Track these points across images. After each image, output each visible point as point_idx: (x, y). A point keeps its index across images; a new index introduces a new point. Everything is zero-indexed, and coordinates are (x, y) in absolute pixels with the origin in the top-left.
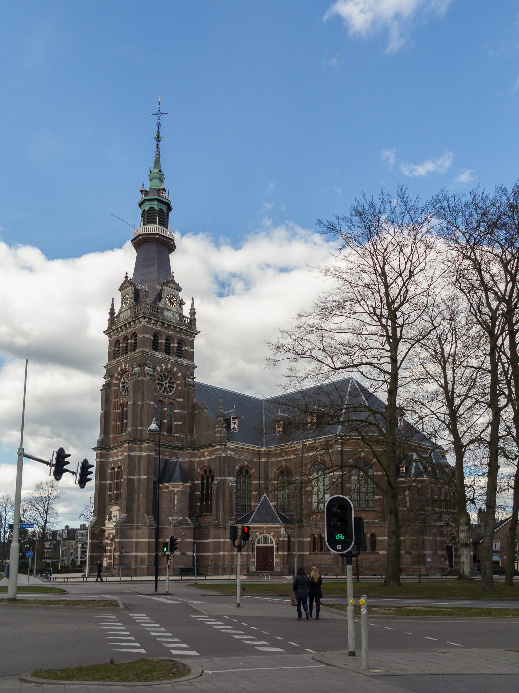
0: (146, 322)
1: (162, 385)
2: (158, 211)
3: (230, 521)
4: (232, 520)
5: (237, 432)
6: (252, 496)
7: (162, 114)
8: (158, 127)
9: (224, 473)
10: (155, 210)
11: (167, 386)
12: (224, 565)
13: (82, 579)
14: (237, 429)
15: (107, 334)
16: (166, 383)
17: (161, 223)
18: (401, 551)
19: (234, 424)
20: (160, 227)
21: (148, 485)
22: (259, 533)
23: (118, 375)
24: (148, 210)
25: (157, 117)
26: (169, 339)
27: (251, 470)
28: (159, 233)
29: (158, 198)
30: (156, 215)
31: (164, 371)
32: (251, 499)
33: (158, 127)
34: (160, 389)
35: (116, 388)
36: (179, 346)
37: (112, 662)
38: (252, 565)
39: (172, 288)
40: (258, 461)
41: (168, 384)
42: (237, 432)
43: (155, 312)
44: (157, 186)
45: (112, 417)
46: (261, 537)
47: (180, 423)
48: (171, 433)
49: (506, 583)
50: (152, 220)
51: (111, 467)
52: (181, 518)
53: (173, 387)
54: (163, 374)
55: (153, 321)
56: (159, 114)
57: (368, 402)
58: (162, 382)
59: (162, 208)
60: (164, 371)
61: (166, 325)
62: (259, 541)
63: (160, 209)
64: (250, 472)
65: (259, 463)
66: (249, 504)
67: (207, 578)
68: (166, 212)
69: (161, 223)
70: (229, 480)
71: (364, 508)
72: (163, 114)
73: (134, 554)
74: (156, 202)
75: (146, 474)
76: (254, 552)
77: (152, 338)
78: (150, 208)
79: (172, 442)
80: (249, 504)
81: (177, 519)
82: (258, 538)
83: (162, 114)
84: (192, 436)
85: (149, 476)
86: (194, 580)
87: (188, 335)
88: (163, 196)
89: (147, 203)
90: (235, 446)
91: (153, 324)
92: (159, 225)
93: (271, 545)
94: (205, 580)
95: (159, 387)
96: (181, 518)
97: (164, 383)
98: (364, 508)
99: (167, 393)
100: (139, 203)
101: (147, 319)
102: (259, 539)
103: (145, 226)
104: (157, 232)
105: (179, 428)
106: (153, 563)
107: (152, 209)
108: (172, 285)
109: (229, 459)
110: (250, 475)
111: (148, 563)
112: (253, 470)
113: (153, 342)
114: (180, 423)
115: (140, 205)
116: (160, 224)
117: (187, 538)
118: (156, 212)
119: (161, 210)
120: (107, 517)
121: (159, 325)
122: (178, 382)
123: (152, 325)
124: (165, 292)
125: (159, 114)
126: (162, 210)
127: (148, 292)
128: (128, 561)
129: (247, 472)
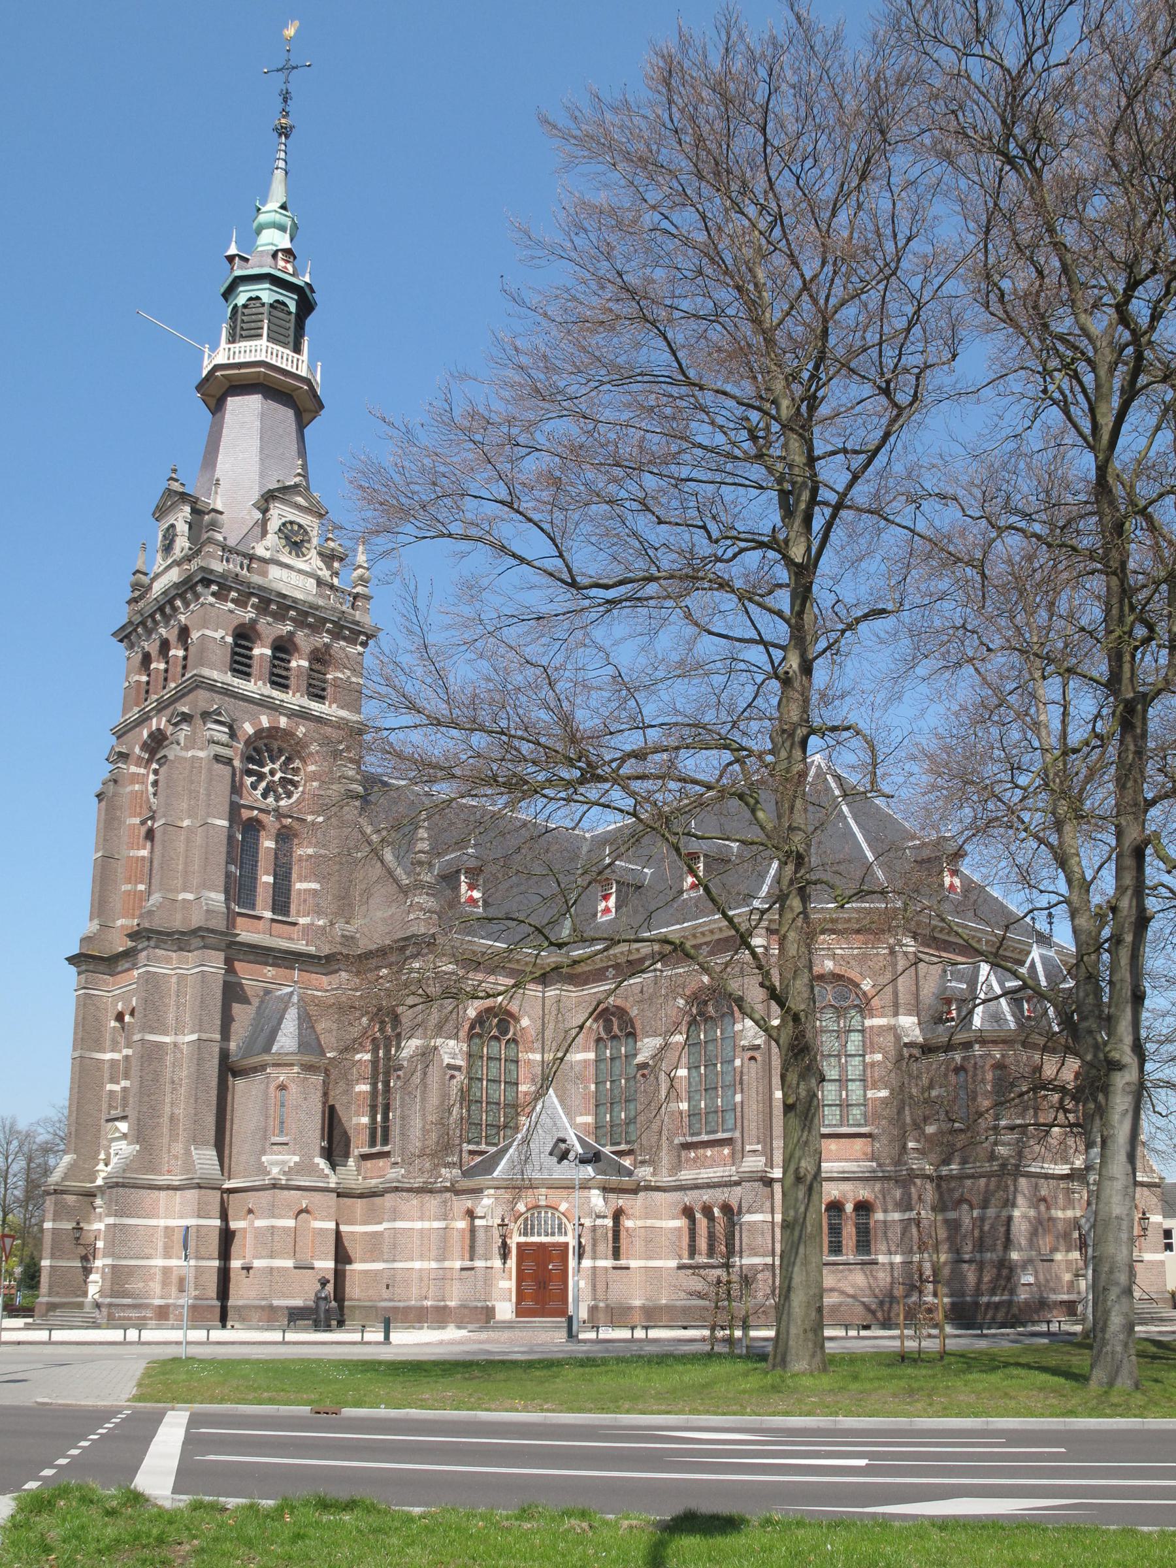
0: (214, 594)
1: (261, 777)
2: (271, 306)
3: (443, 1171)
4: (448, 1165)
7: (294, 68)
8: (285, 100)
10: (263, 305)
11: (276, 778)
13: (47, 1332)
15: (121, 641)
16: (272, 773)
20: (271, 345)
21: (200, 1061)
23: (142, 749)
24: (245, 306)
25: (281, 76)
26: (283, 648)
29: (273, 272)
31: (267, 737)
33: (285, 100)
34: (254, 786)
35: (137, 787)
36: (317, 667)
38: (504, 1300)
39: (298, 507)
41: (279, 775)
43: (242, 568)
45: (120, 870)
47: (315, 886)
48: (286, 913)
49: (331, 922)
50: (253, 332)
51: (115, 1013)
52: (297, 1159)
53: (295, 784)
54: (266, 745)
55: (234, 594)
56: (288, 68)
57: (888, 867)
58: (263, 767)
60: (267, 737)
61: (274, 607)
62: (526, 1229)
67: (58, 1335)
68: (293, 308)
71: (835, 1125)
73: (159, 1262)
75: (197, 1028)
76: (509, 1261)
77: (229, 639)
78: (251, 299)
79: (291, 939)
81: (284, 1163)
83: (294, 68)
84: (347, 923)
85: (204, 1036)
86: (178, 1343)
87: (345, 639)
91: (233, 601)
92: (270, 339)
93: (562, 1239)
94: (50, 1343)
95: (249, 780)
96: (297, 1159)
97: (266, 770)
98: (835, 1125)
99: (277, 800)
100: (222, 290)
101: (214, 588)
103: (231, 346)
104: (263, 358)
105: (311, 901)
106: (212, 1290)
108: (300, 500)
110: (514, 1034)
111: (196, 1289)
113: (235, 653)
114: (315, 886)
117: (316, 1219)
118: (265, 310)
119: (278, 305)
120: (102, 1156)
121: (253, 606)
122: (312, 768)
123: (231, 605)
124: (275, 517)
125: (288, 68)
127: (221, 513)
128: (141, 1285)
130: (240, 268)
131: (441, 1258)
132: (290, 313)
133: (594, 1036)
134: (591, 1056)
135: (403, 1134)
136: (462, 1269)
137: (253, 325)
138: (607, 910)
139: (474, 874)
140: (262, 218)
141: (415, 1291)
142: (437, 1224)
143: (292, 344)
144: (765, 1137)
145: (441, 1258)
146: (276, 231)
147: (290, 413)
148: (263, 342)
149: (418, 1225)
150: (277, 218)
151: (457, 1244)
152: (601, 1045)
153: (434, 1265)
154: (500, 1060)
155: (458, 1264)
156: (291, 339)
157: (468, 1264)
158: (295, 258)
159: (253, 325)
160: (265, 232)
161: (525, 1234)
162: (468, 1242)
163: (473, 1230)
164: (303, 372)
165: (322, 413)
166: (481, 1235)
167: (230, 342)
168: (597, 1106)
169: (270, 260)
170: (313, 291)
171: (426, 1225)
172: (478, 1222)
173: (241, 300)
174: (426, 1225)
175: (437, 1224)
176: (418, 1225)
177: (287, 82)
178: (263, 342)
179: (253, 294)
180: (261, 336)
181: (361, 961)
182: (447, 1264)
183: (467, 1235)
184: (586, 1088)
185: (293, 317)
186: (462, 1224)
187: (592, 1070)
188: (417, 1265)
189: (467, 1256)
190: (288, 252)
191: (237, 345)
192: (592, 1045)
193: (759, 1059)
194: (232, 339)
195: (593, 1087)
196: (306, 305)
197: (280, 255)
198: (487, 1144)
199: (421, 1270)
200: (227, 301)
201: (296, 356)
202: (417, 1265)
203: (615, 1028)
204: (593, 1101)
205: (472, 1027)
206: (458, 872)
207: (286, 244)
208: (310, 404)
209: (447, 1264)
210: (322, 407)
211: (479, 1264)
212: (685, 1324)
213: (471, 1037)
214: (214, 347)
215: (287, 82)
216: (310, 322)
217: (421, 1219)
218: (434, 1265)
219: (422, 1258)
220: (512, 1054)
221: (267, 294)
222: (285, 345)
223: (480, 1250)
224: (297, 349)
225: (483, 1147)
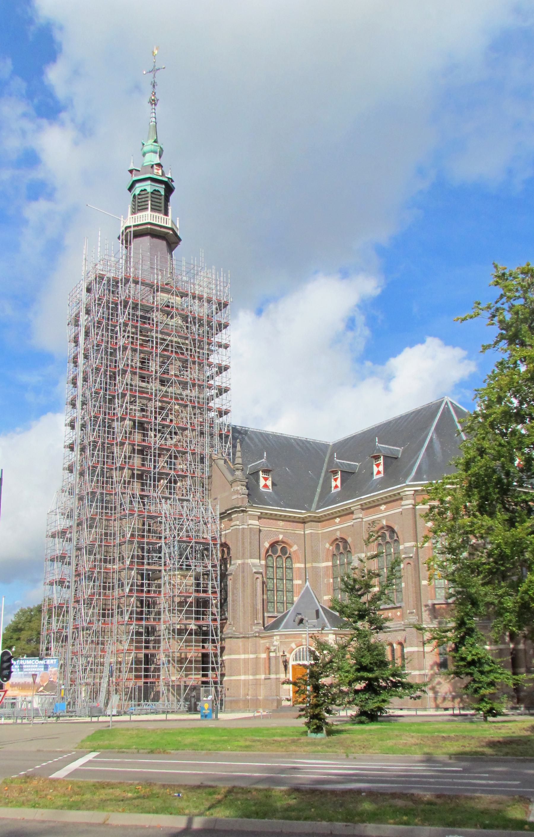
2: (152, 193)
3: (254, 627)
5: (271, 491)
6: (295, 587)
7: (157, 70)
8: (154, 86)
9: (243, 554)
12: (248, 695)
14: (270, 487)
17: (154, 209)
18: (520, 667)
19: (266, 479)
22: (296, 644)
24: (139, 195)
25: (152, 74)
27: (291, 547)
28: (152, 222)
30: (149, 199)
32: (293, 592)
33: (154, 86)
37: (331, 833)
40: (303, 533)
42: (271, 491)
44: (151, 161)
46: (300, 651)
56: (154, 71)
59: (157, 189)
62: (296, 657)
63: (155, 190)
64: (290, 551)
65: (305, 537)
66: (289, 599)
68: (163, 193)
69: (154, 209)
70: (252, 563)
72: (159, 69)
74: (149, 182)
76: (287, 675)
78: (142, 191)
80: (289, 599)
82: (294, 653)
83: (157, 70)
86: (109, 722)
88: (158, 173)
89: (137, 185)
90: (261, 513)
100: (128, 187)
102: (296, 655)
103: (134, 216)
104: (149, 221)
107: (156, 193)
109: (250, 532)
110: (290, 554)
112: (295, 548)
115: (130, 189)
116: (153, 210)
118: (149, 195)
119: (155, 192)
126: (158, 191)
129: (284, 551)
130: (135, 176)
131: (255, 673)
132: (161, 195)
133: (331, 554)
134: (330, 564)
135: (234, 610)
136: (265, 679)
137: (143, 204)
138: (336, 487)
139: (266, 471)
140: (146, 149)
141: (242, 692)
142: (252, 656)
143: (163, 211)
144: (417, 605)
145: (255, 673)
146: (152, 154)
147: (164, 243)
148: (149, 212)
149: (243, 656)
150: (152, 148)
151: (262, 667)
152: (335, 557)
153: (251, 677)
154: (283, 568)
155: (263, 677)
156: (163, 208)
157: (268, 676)
158: (162, 167)
159: (143, 204)
160: (147, 155)
161: (296, 660)
162: (267, 665)
163: (269, 658)
164: (169, 225)
165: (181, 243)
166: (273, 661)
167: (132, 214)
168: (334, 590)
169: (150, 169)
170: (172, 181)
171: (246, 656)
172: (272, 654)
173: (137, 191)
174: (246, 656)
175: (252, 656)
176: (243, 656)
177: (154, 77)
178: (149, 212)
179: (143, 188)
180: (147, 208)
181: (213, 427)
182: (258, 677)
183: (267, 661)
184: (328, 581)
185: (163, 198)
186: (264, 656)
187: (331, 571)
188: (243, 677)
189: (267, 672)
190: (159, 165)
191: (136, 215)
192: (330, 558)
193: (412, 564)
194: (134, 213)
195: (331, 580)
196: (169, 190)
197: (155, 166)
198: (278, 612)
199: (244, 680)
200: (130, 192)
201: (165, 217)
202: (243, 677)
203: (341, 548)
204: (331, 588)
205: (267, 551)
206: (258, 472)
207: (158, 161)
208: (173, 239)
209: (258, 677)
210: (180, 240)
211: (273, 676)
212: (401, 707)
213: (266, 558)
214: (125, 218)
215: (154, 77)
216: (172, 197)
217: (244, 653)
218: (251, 677)
219: (245, 673)
220: (288, 565)
221: (149, 187)
222: (159, 211)
223: (273, 669)
224: (166, 214)
225: (276, 614)
